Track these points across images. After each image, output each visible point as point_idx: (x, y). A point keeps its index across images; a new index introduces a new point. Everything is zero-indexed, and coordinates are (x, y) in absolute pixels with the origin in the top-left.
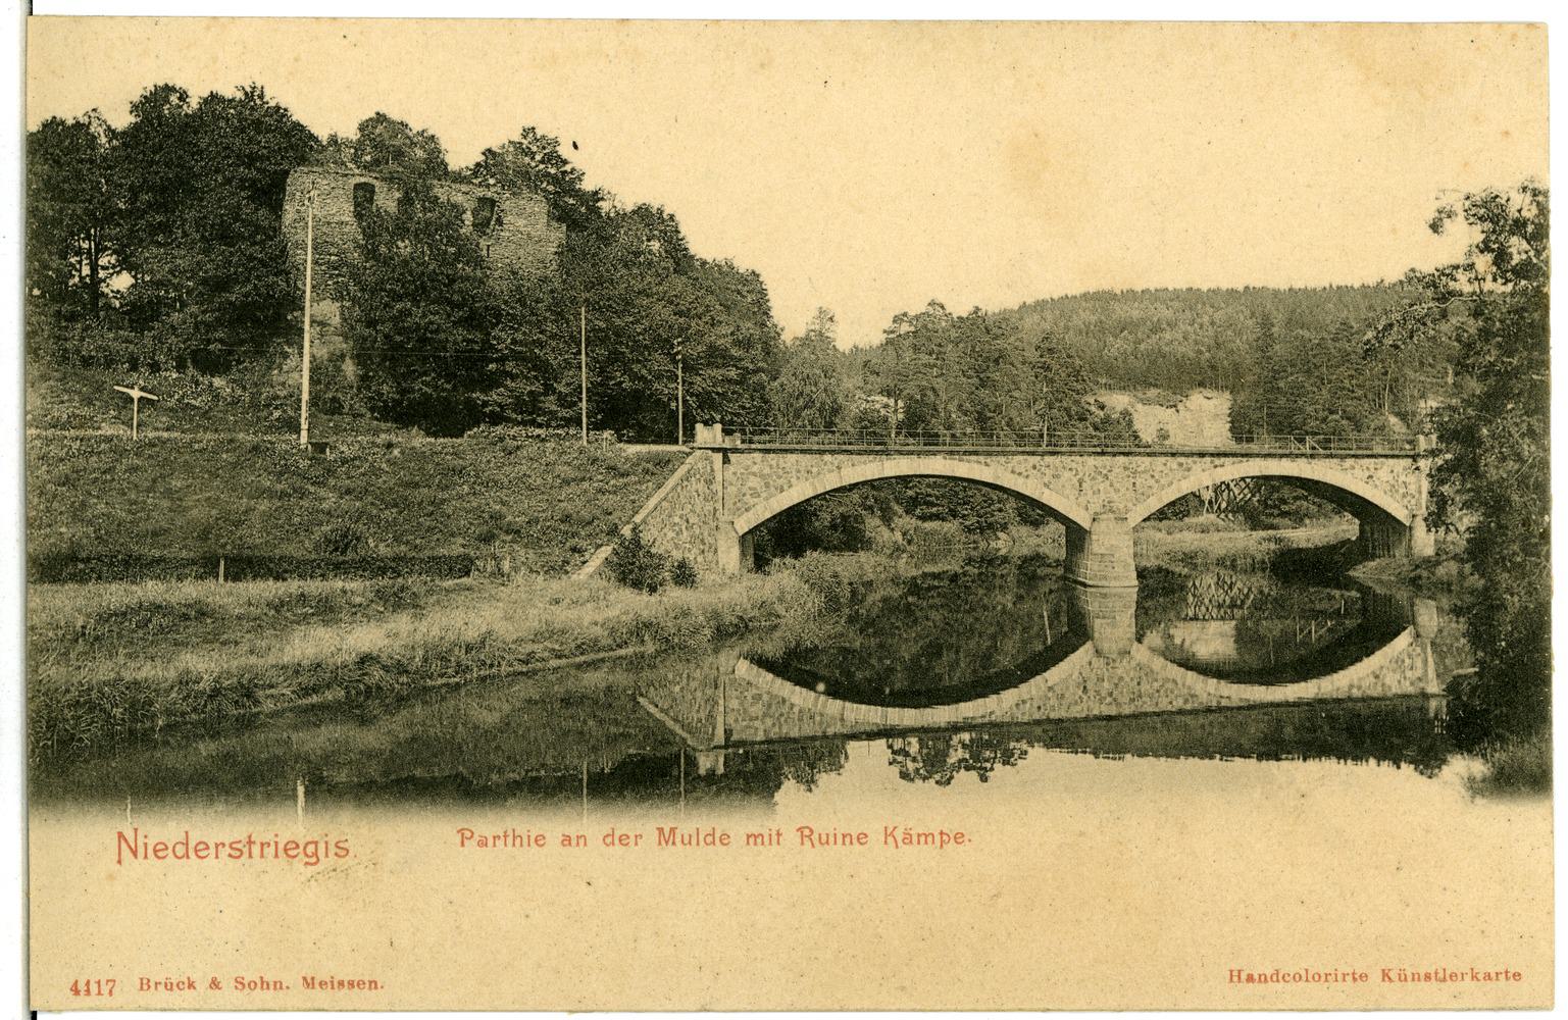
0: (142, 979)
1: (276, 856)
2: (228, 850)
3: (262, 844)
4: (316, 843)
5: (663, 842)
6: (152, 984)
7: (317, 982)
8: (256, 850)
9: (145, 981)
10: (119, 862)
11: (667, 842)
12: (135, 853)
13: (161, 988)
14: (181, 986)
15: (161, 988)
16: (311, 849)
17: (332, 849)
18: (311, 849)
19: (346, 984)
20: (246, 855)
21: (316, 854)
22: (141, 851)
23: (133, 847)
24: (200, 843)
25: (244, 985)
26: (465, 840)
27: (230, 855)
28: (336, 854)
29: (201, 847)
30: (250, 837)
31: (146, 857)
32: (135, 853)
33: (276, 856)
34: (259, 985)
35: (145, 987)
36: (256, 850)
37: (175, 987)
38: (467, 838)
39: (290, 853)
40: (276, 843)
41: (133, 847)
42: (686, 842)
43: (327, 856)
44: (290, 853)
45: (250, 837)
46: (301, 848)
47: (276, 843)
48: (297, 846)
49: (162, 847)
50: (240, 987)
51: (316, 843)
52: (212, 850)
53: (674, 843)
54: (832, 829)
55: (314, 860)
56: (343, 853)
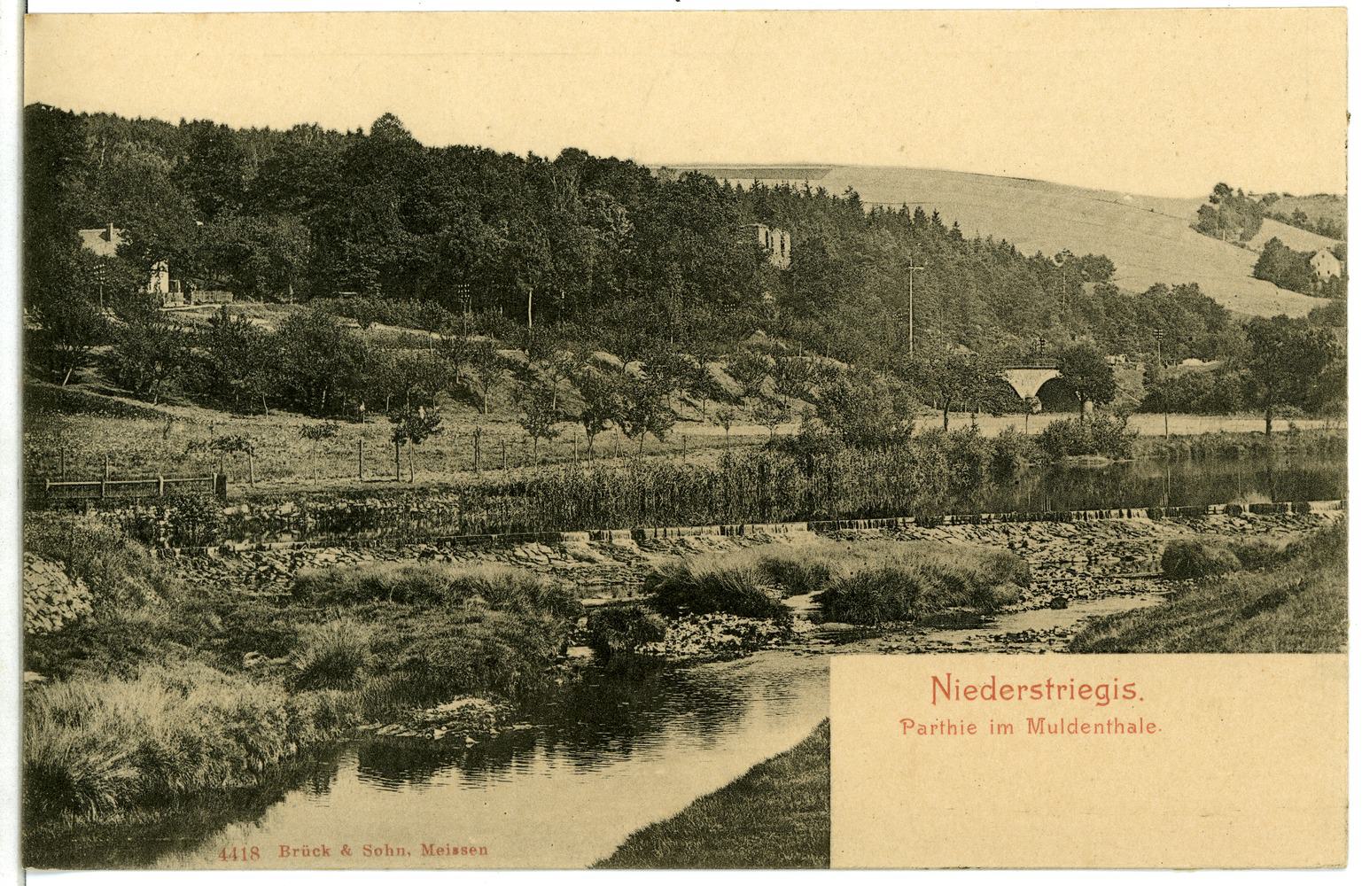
0: (282, 847)
1: (1072, 698)
2: (1029, 693)
3: (1059, 688)
4: (1107, 686)
5: (1032, 731)
6: (291, 851)
7: (435, 848)
8: (1054, 692)
9: (285, 849)
10: (934, 703)
11: (1036, 732)
12: (948, 695)
13: (299, 854)
14: (317, 853)
15: (299, 854)
16: (1102, 692)
17: (1121, 692)
18: (1102, 692)
19: (459, 850)
20: (1045, 695)
21: (1106, 696)
22: (953, 694)
23: (946, 688)
24: (1083, 686)
25: (370, 851)
26: (991, 684)
27: (1032, 697)
28: (1124, 696)
29: (1084, 689)
30: (1049, 681)
31: (957, 698)
32: (948, 695)
33: (1072, 698)
34: (384, 852)
35: (285, 854)
36: (1054, 692)
37: (311, 853)
38: (989, 687)
39: (969, 696)
40: (1072, 686)
41: (946, 688)
42: (1052, 730)
43: (1116, 698)
44: (969, 696)
45: (1049, 681)
46: (979, 690)
47: (1072, 686)
48: (1090, 690)
49: (972, 689)
50: (367, 853)
51: (1107, 686)
52: (1016, 693)
53: (1042, 732)
54: (1069, 681)
55: (1104, 701)
56: (1131, 695)
